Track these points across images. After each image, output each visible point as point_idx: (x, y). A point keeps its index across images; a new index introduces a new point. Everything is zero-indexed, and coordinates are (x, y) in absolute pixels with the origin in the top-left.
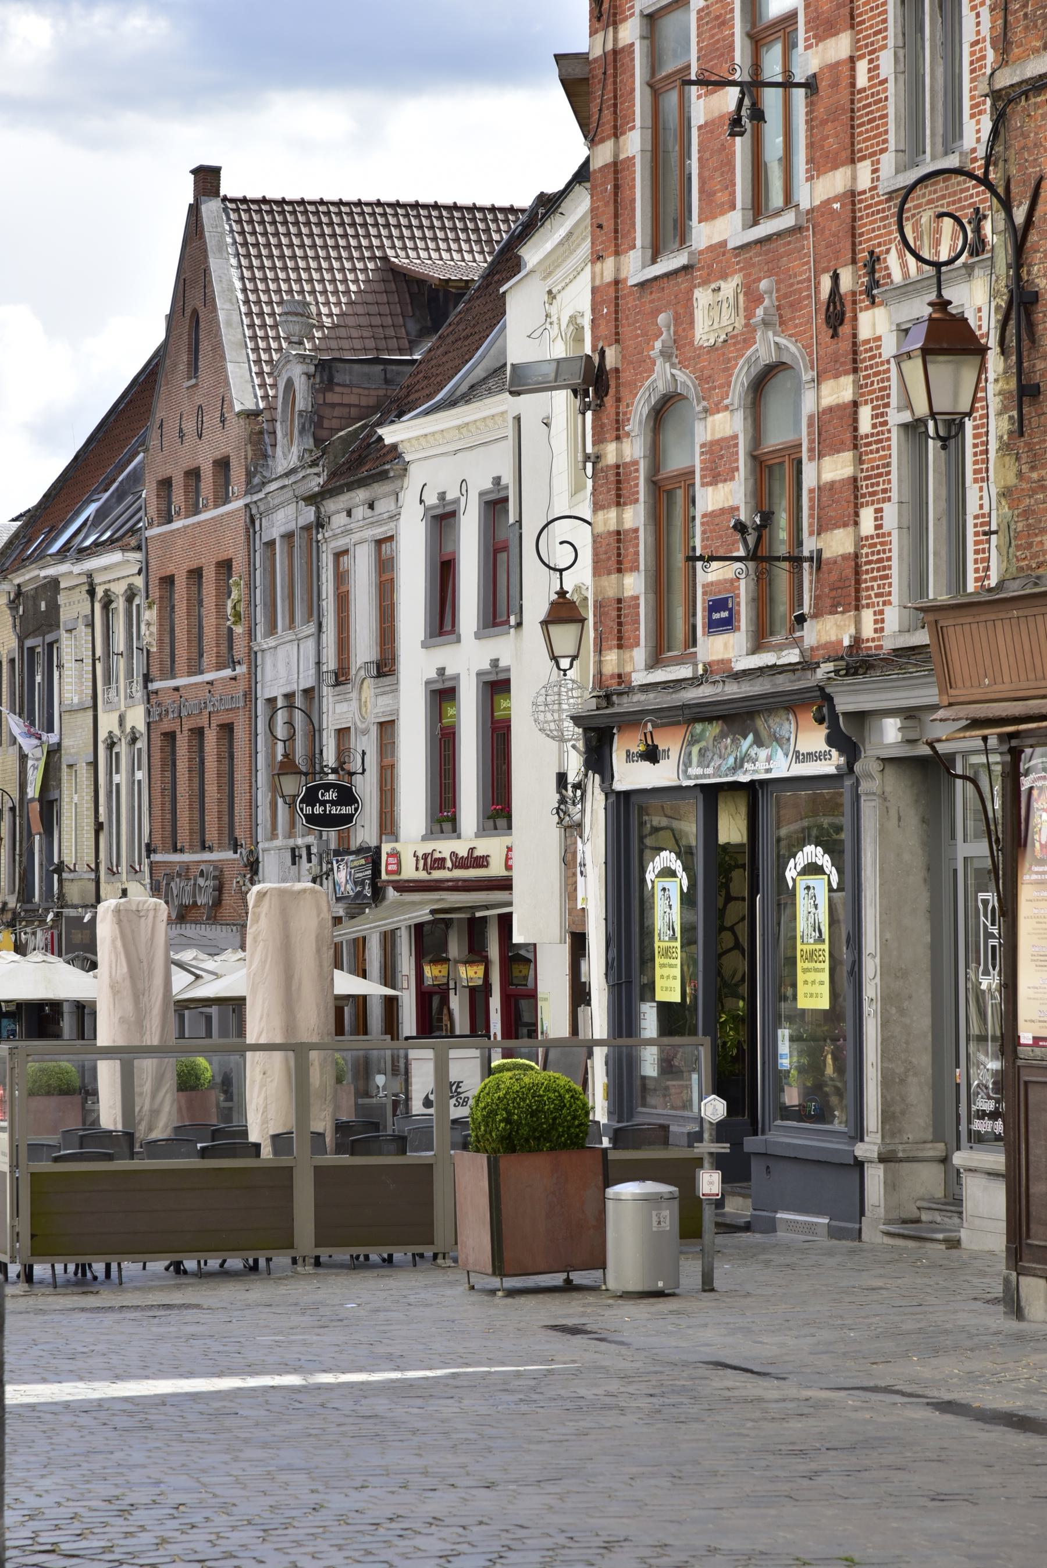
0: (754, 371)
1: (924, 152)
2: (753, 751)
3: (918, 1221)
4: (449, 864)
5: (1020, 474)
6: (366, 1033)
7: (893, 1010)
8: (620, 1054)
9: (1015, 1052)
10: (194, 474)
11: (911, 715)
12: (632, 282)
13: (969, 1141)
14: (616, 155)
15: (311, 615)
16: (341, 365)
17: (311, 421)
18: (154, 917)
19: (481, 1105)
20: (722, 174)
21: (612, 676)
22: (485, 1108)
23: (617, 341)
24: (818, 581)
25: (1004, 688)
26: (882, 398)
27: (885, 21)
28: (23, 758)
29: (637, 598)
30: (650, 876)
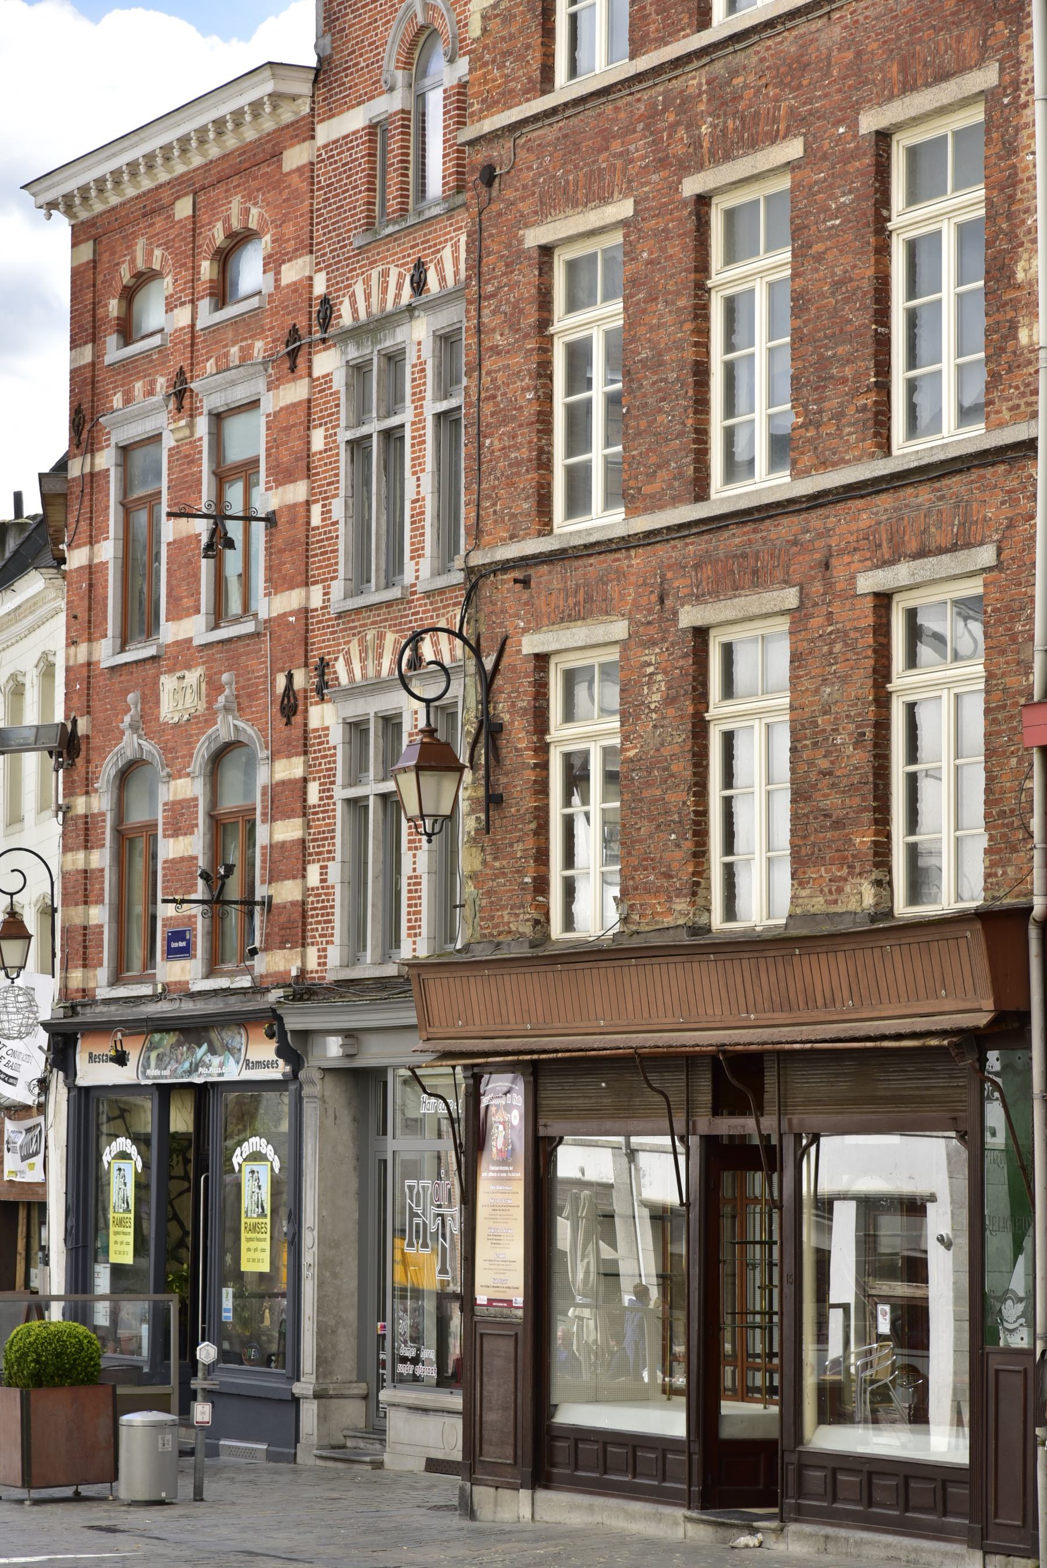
0: (214, 747)
1: (369, 581)
2: (208, 1058)
3: (344, 1447)
5: (484, 863)
7: (328, 1274)
8: (76, 1307)
9: (473, 1310)
11: (349, 1034)
12: (103, 665)
13: (393, 1381)
14: (91, 559)
19: (15, 1348)
20: (188, 584)
21: (77, 991)
23: (88, 713)
24: (268, 921)
25: (474, 1029)
26: (329, 776)
27: (337, 475)
29: (101, 926)
30: (106, 1158)
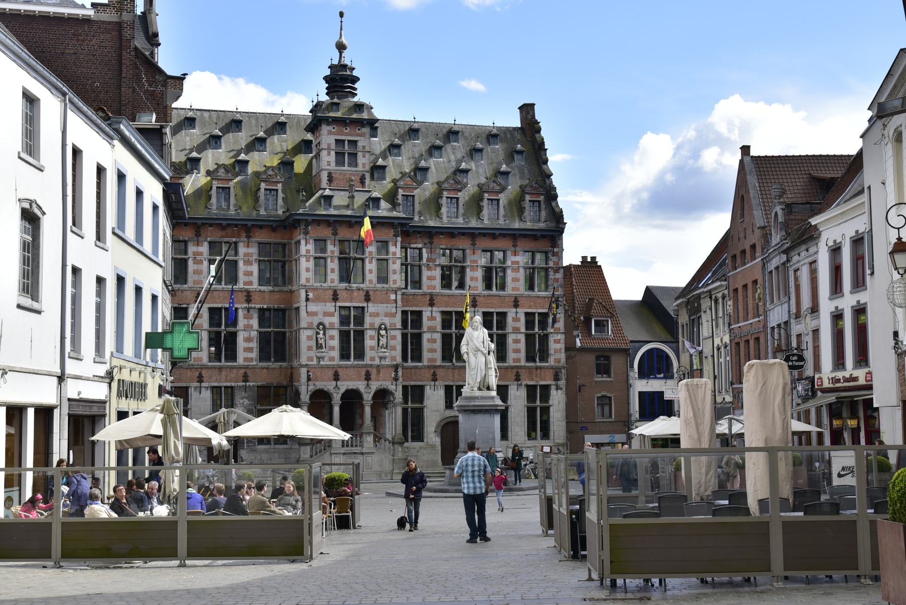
4: (842, 381)
6: (810, 445)
10: (743, 252)
15: (786, 295)
16: (794, 205)
17: (784, 226)
18: (705, 388)
22: (899, 491)
28: (691, 356)
